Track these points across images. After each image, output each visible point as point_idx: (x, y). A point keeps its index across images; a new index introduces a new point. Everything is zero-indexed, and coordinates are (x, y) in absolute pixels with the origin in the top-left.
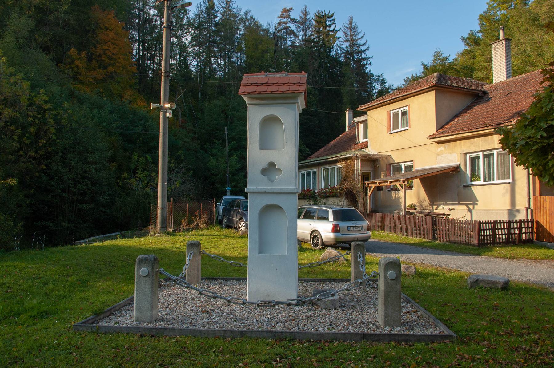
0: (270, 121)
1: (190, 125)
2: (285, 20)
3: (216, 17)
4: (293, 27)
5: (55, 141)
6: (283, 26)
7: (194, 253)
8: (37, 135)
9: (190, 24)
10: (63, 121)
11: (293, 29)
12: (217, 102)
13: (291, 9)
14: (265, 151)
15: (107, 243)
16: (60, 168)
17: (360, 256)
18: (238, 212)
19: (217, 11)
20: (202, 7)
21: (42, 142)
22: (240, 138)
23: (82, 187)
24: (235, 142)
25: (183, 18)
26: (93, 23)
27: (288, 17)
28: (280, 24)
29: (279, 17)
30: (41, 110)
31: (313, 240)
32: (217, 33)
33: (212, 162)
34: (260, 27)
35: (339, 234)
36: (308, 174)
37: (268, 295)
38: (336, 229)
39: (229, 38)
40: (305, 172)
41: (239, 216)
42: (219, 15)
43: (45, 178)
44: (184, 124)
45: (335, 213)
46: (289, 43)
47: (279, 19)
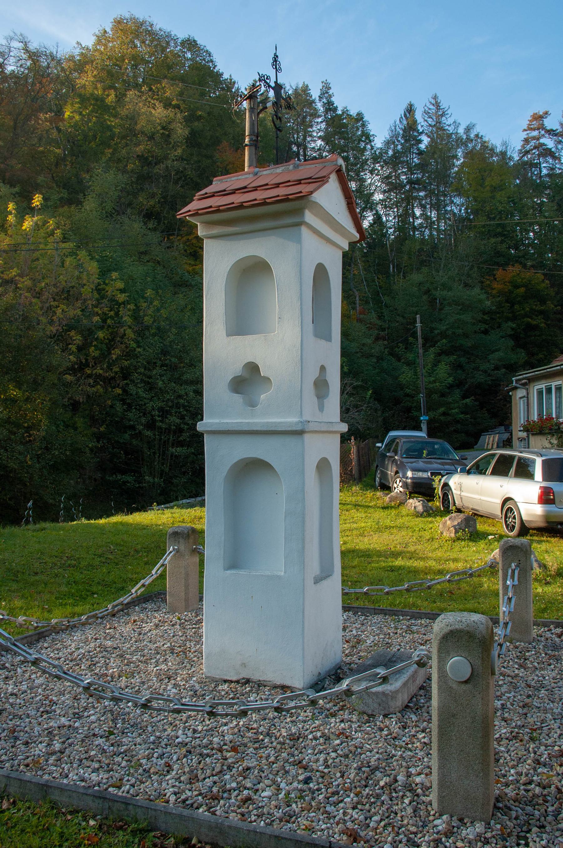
0: (252, 272)
1: (373, 317)
2: (535, 133)
3: (420, 141)
4: (549, 142)
5: (135, 350)
6: (533, 143)
7: (178, 551)
8: (110, 344)
9: (376, 159)
10: (146, 318)
11: (550, 147)
12: (416, 277)
13: (546, 113)
14: (238, 340)
15: (102, 521)
16: (141, 392)
17: (513, 571)
18: (394, 461)
19: (422, 133)
20: (398, 129)
21: (116, 353)
22: (454, 333)
23: (174, 420)
24: (444, 341)
25: (365, 149)
26: (220, 170)
27: (542, 127)
28: (526, 141)
29: (525, 130)
30: (115, 304)
31: (506, 517)
32: (422, 167)
33: (406, 375)
34: (492, 150)
35: (552, 508)
36: (549, 390)
37: (244, 665)
38: (546, 497)
39: (442, 176)
40: (543, 386)
41: (395, 469)
42: (425, 140)
43: (119, 407)
44: (362, 316)
45: (548, 465)
46: (545, 172)
47: (526, 133)
